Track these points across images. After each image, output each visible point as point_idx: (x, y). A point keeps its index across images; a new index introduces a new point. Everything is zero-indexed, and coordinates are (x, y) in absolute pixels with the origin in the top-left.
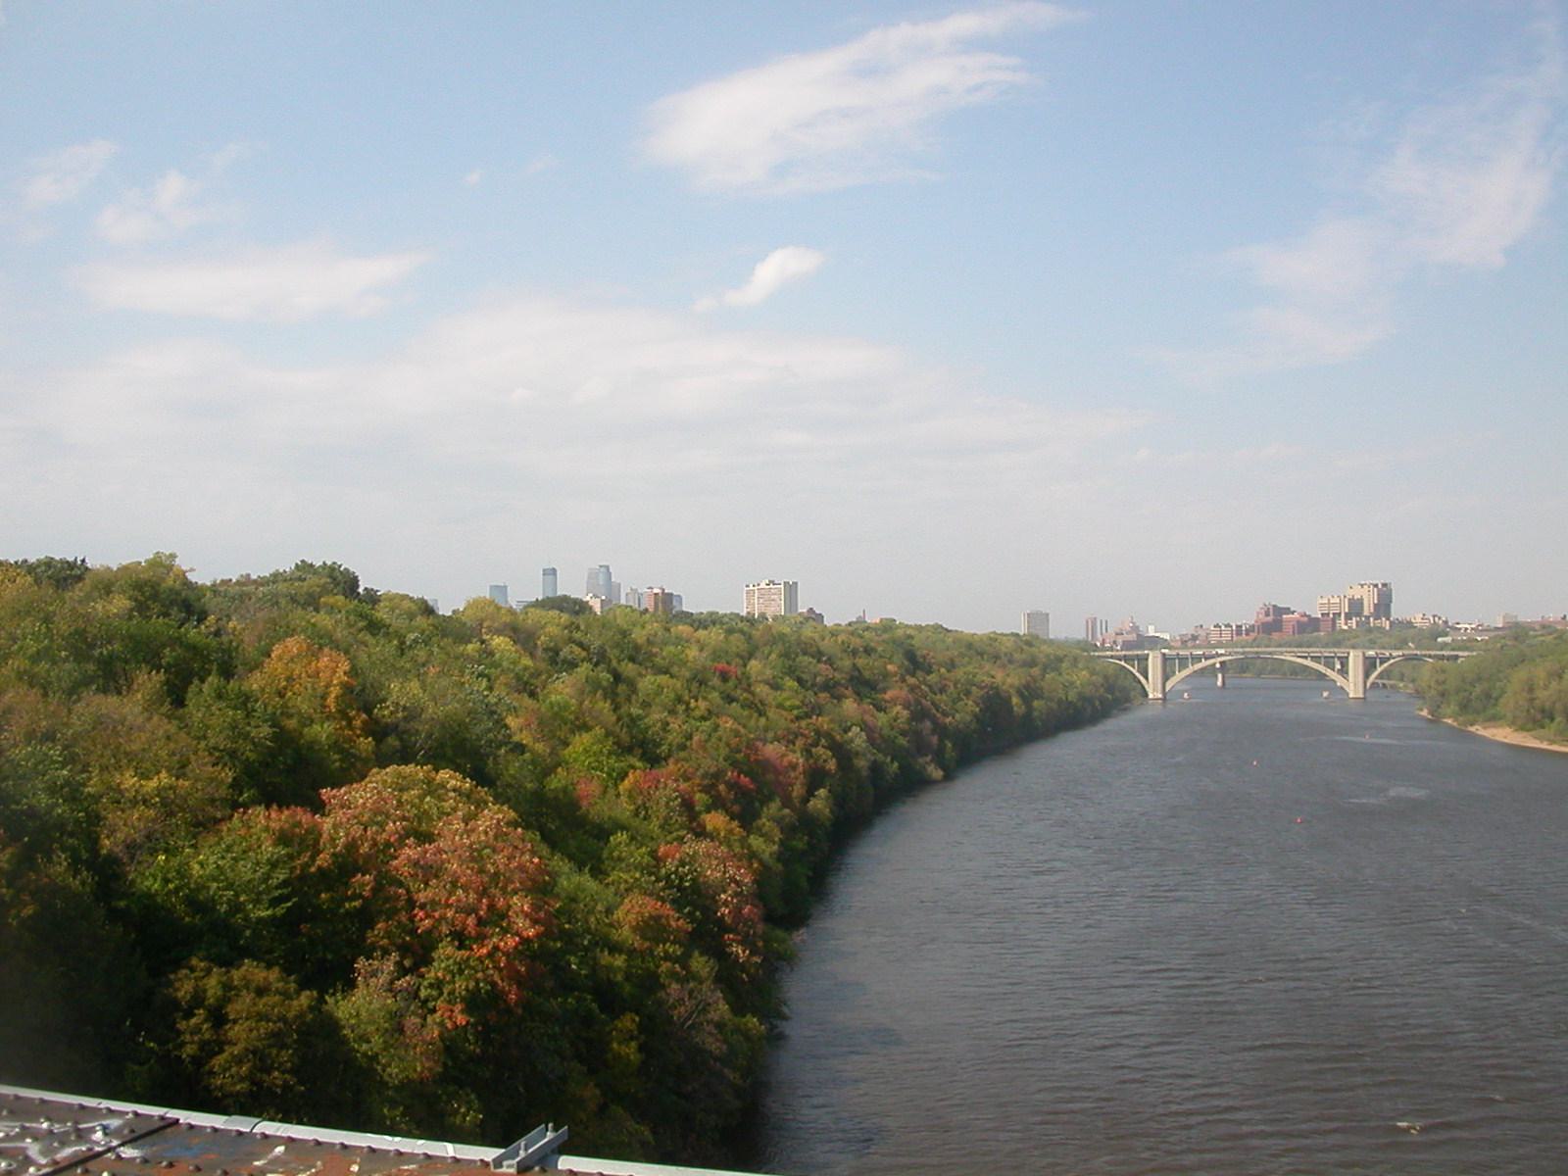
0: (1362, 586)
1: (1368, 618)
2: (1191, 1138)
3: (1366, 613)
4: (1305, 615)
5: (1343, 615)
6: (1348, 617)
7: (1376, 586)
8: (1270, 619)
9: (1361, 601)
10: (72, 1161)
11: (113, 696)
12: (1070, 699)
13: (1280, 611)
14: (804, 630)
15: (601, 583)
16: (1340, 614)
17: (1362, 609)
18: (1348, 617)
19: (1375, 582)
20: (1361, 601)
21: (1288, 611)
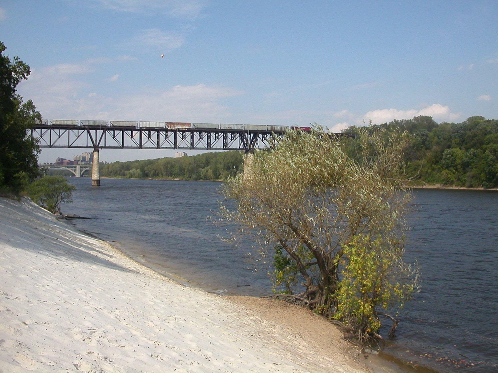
0: (86, 153)
1: (87, 162)
2: (455, 240)
3: (87, 160)
4: (69, 160)
5: (80, 161)
6: (82, 161)
7: (90, 153)
8: (60, 161)
9: (85, 158)
10: (87, 124)
11: (61, 180)
12: (269, 130)
13: (62, 159)
14: (90, 367)
15: (97, 268)
16: (79, 161)
17: (86, 160)
18: (82, 161)
19: (89, 152)
20: (85, 158)
21: (65, 159)
